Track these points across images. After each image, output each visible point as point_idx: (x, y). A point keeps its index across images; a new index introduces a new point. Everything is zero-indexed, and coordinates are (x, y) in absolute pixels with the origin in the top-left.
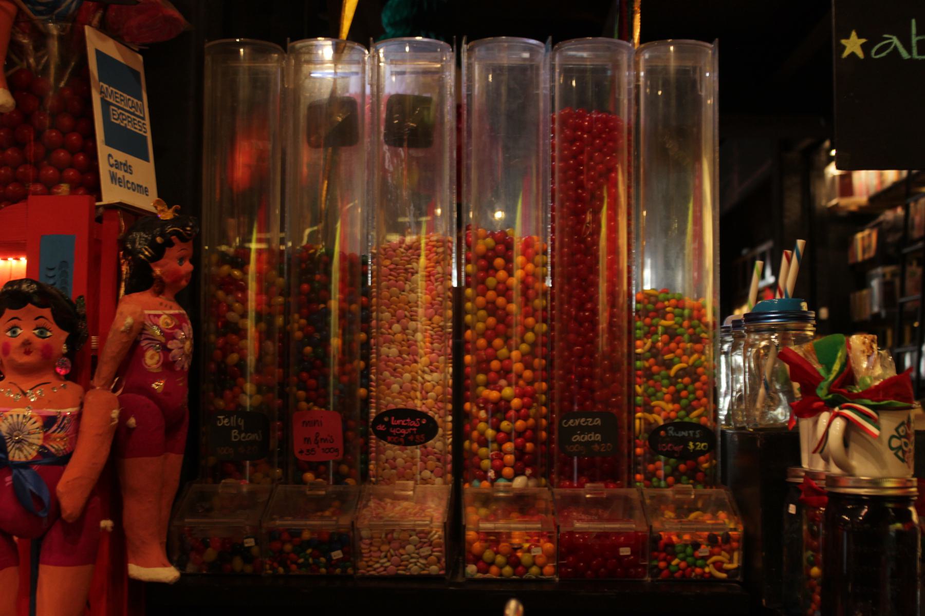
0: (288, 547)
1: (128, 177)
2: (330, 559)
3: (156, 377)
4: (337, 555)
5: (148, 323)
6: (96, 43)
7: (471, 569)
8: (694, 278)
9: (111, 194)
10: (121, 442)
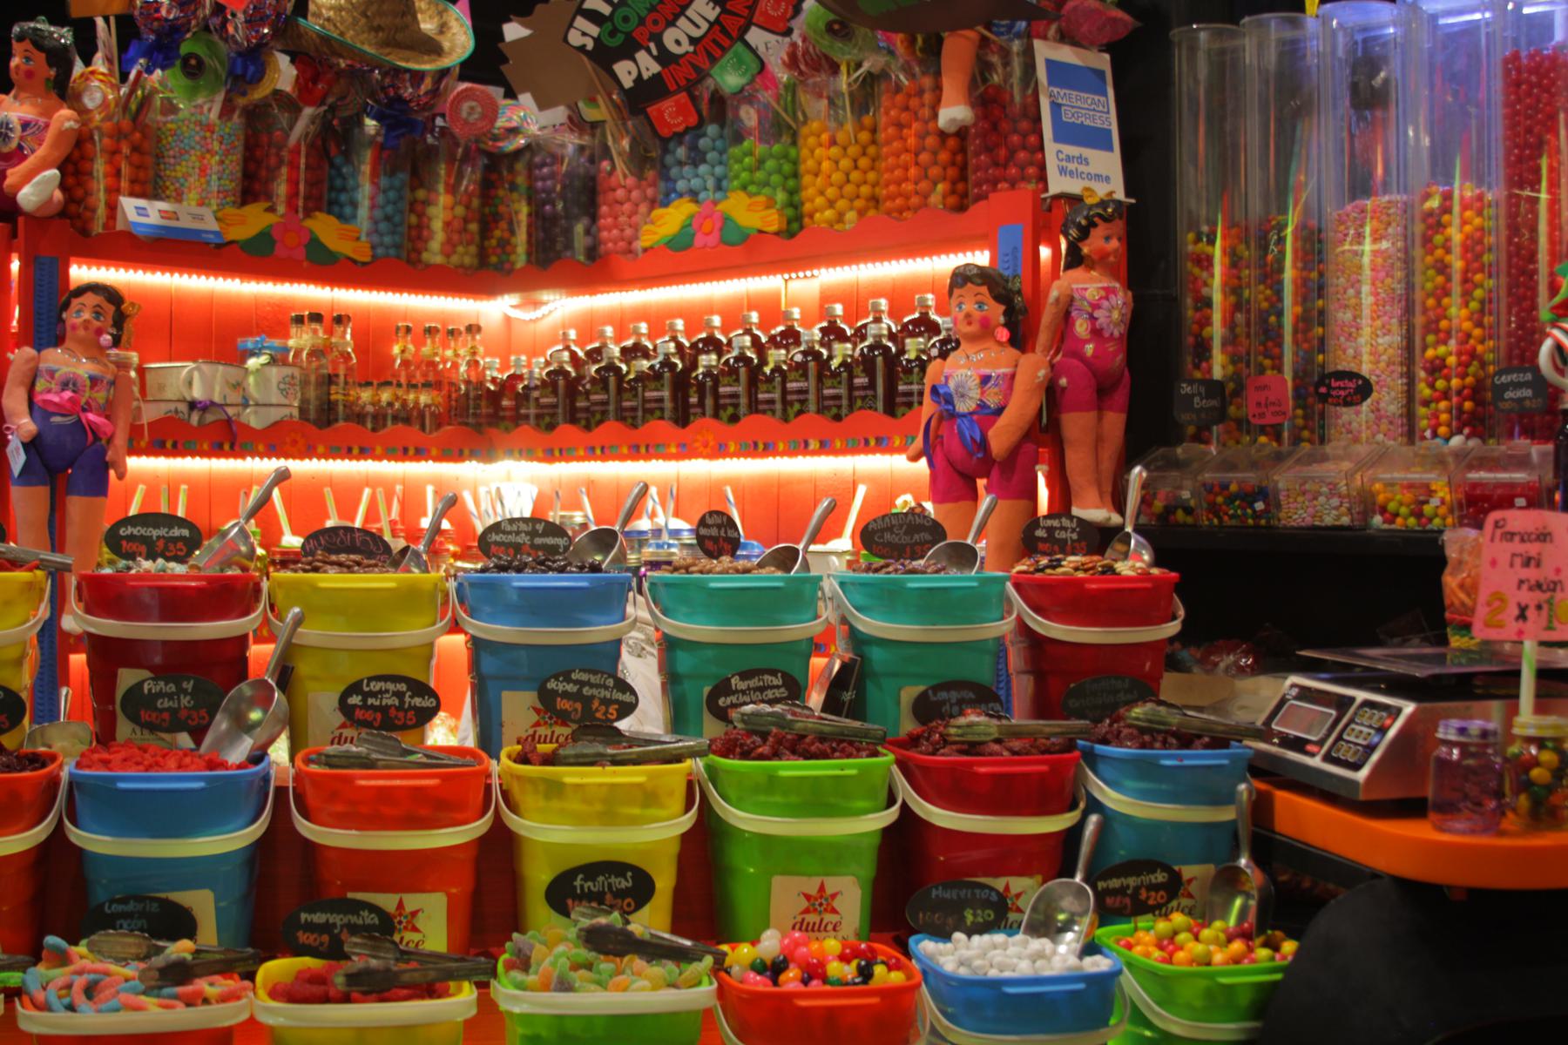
0: (1220, 499)
1: (1082, 168)
2: (1254, 511)
3: (1087, 341)
4: (1259, 506)
5: (1076, 296)
7: (1377, 520)
8: (51, 198)
10: (1052, 394)
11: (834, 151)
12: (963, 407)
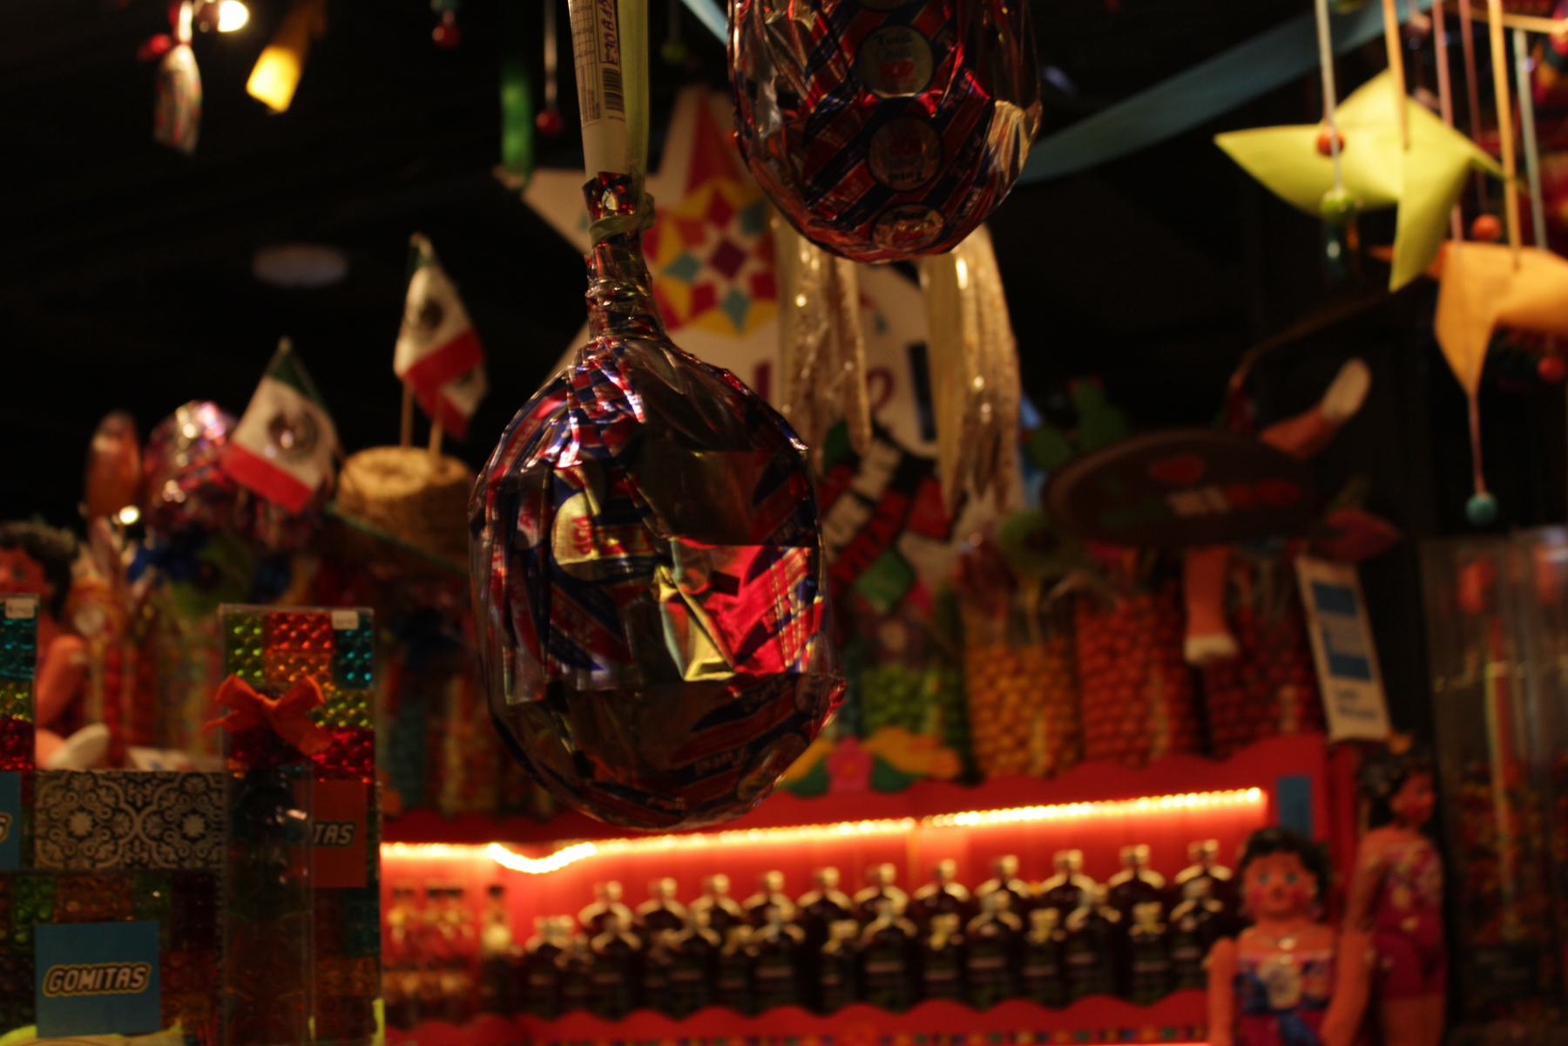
3: (1406, 915)
6: (1311, 572)
9: (1342, 727)
10: (1379, 986)
11: (1022, 682)
12: (1283, 1000)
